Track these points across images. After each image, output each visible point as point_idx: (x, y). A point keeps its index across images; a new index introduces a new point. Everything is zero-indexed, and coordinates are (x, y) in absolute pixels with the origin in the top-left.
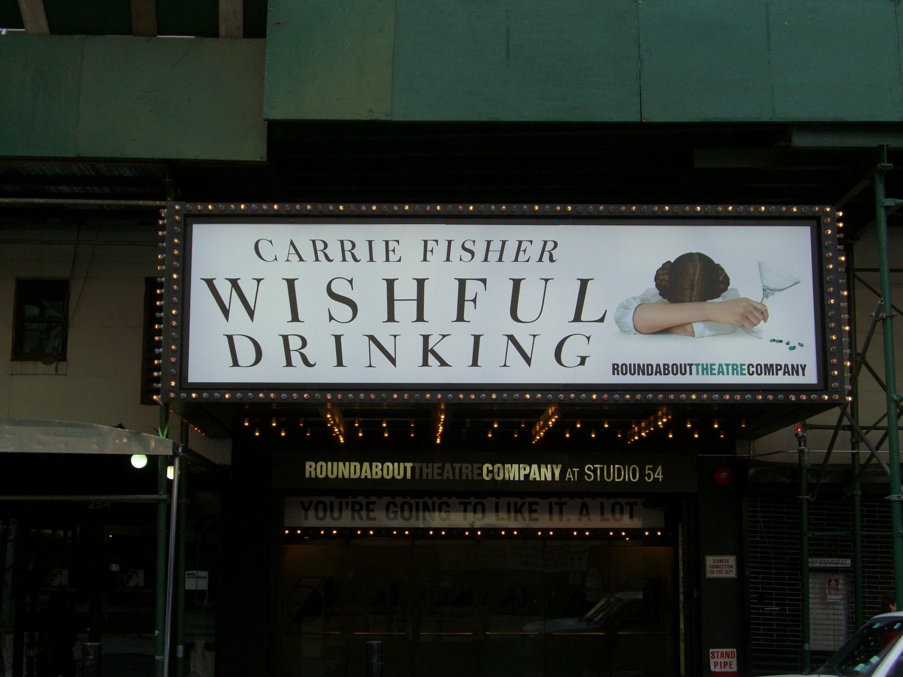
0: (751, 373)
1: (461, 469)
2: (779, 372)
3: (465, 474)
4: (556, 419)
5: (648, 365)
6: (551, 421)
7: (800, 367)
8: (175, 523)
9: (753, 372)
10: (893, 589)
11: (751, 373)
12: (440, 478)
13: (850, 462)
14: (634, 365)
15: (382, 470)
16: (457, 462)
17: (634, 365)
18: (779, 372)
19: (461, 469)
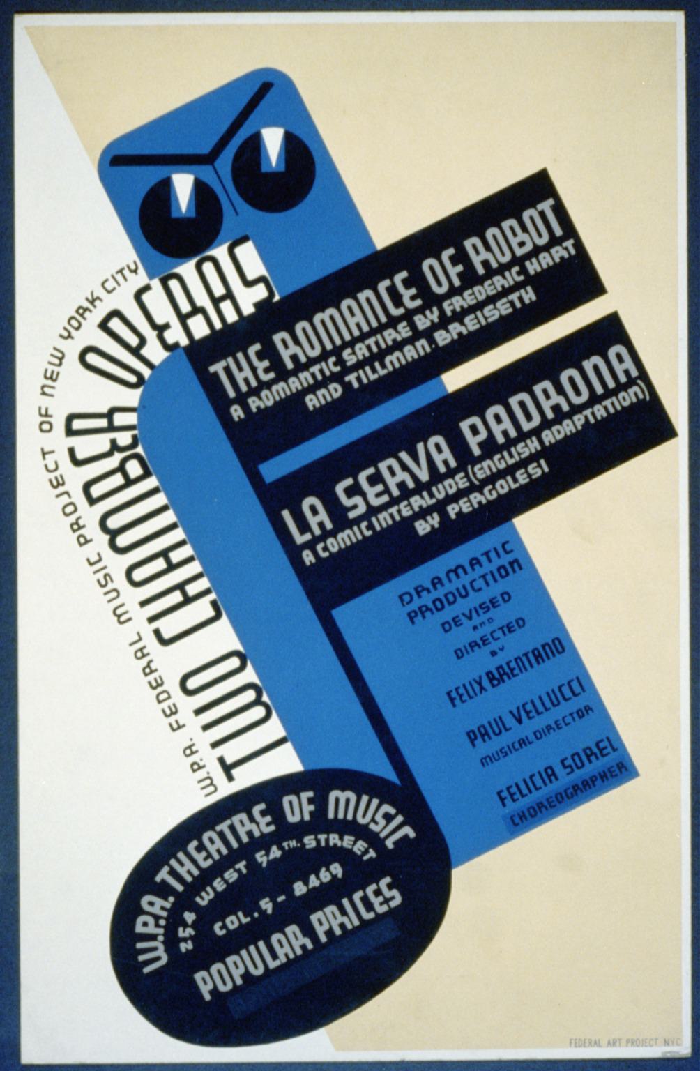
0: (570, 795)
1: (232, 828)
2: (144, 352)
3: (209, 797)
4: (334, 877)
5: (543, 646)
6: (306, 883)
7: (473, 683)
8: (411, 393)
9: (572, 794)
10: (521, 671)
11: (570, 795)
12: (210, 862)
13: (342, 614)
14: (549, 658)
15: (486, 291)
16: (322, 832)
17: (549, 658)
18: (144, 352)
19: (232, 828)
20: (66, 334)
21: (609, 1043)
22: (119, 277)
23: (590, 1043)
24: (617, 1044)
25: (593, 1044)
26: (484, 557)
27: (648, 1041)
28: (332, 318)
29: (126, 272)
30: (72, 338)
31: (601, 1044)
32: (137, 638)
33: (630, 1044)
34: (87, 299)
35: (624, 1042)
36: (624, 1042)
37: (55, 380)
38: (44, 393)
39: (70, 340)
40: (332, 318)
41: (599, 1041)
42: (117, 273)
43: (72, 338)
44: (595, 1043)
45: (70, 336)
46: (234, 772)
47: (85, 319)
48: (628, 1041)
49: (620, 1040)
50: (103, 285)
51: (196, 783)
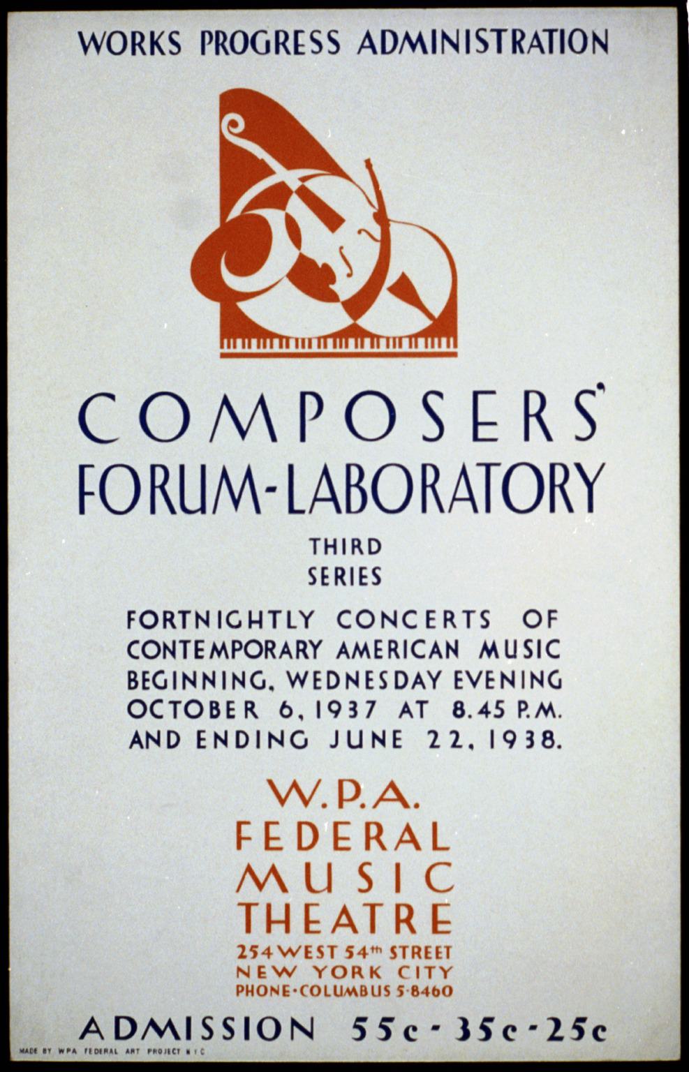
32: (292, 624)
34: (372, 968)
42: (181, 641)
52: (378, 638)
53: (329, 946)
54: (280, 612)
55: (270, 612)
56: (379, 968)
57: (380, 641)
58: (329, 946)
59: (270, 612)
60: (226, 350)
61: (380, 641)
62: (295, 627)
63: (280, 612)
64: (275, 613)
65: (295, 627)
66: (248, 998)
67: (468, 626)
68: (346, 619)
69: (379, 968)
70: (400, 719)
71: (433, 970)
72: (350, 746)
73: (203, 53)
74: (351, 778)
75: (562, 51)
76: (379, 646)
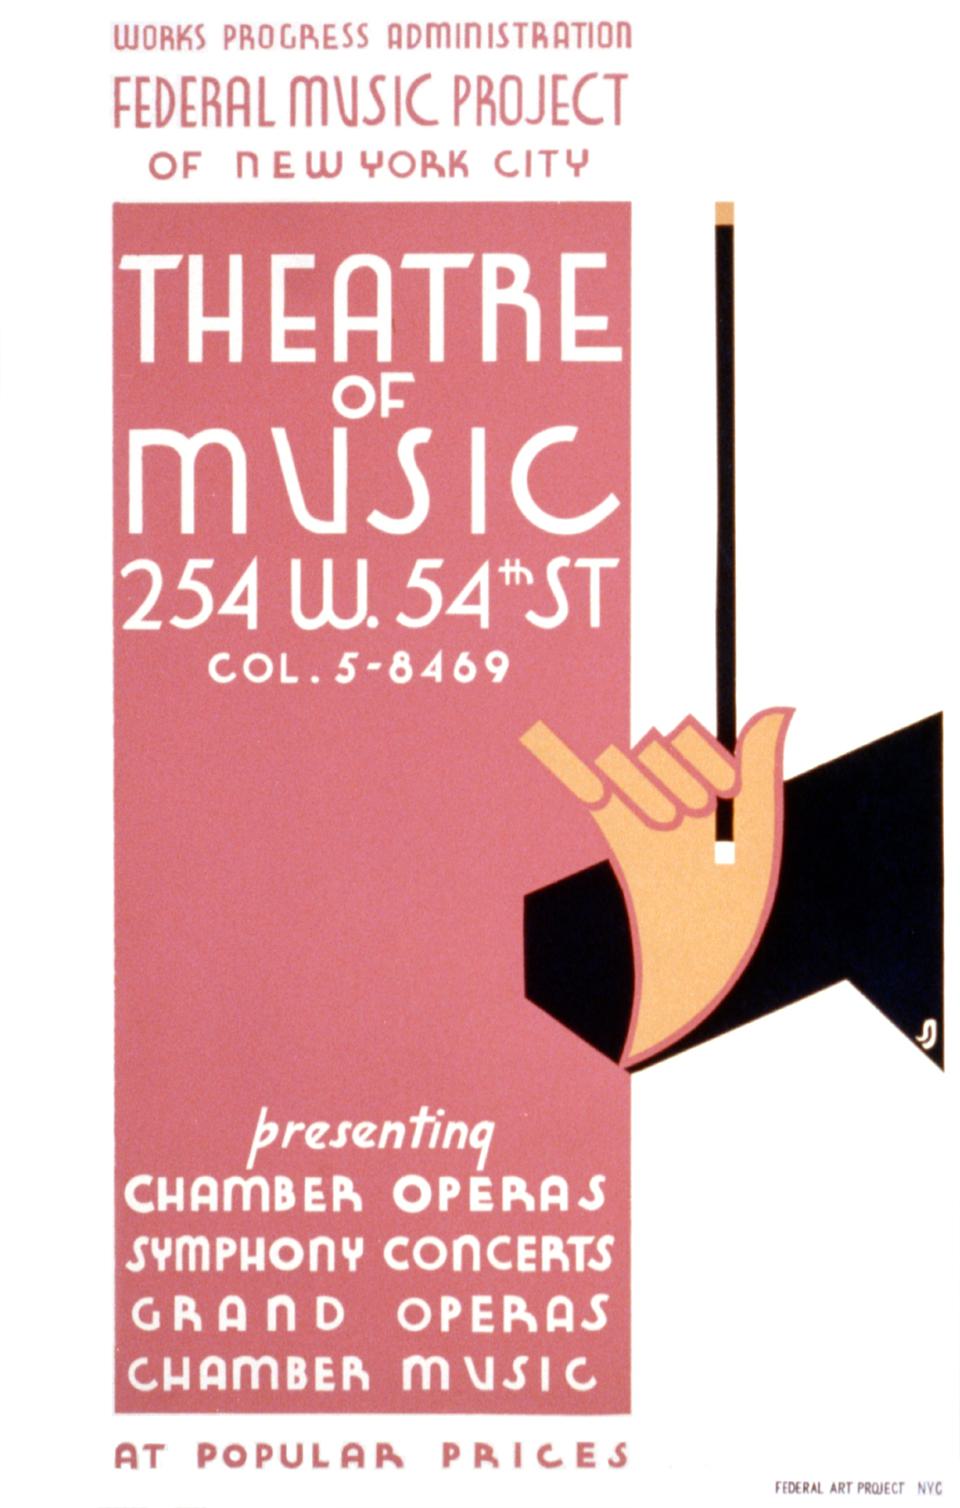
13: (600, 762)
20: (372, 159)
21: (833, 1488)
22: (539, 162)
23: (805, 1489)
24: (846, 1489)
25: (810, 1488)
26: (148, 1453)
27: (890, 1486)
28: (199, 1249)
29: (558, 161)
30: (372, 175)
31: (821, 1489)
32: (267, 118)
33: (863, 1490)
34: (452, 154)
35: (854, 1487)
36: (854, 1487)
37: (326, 46)
38: (240, 155)
39: (366, 172)
40: (199, 1249)
41: (819, 1485)
43: (372, 175)
44: (814, 1488)
45: (372, 169)
46: (544, 157)
47: (424, 174)
48: (860, 1486)
49: (849, 1484)
50: (500, 156)
51: (336, 74)
52: (329, 22)
53: (515, 24)
54: (555, 152)
55: (541, 152)
56: (463, 153)
57: (333, 26)
58: (515, 24)
59: (541, 152)
60: (199, 121)
61: (333, 26)
62: (271, 124)
63: (555, 152)
64: (548, 154)
65: (271, 124)
66: (244, 52)
67: (457, 122)
68: (507, 164)
69: (463, 153)
70: (440, 121)
71: (553, 156)
72: (254, 157)
73: (117, 124)
74: (745, 783)
75: (493, 122)
76: (331, 32)
